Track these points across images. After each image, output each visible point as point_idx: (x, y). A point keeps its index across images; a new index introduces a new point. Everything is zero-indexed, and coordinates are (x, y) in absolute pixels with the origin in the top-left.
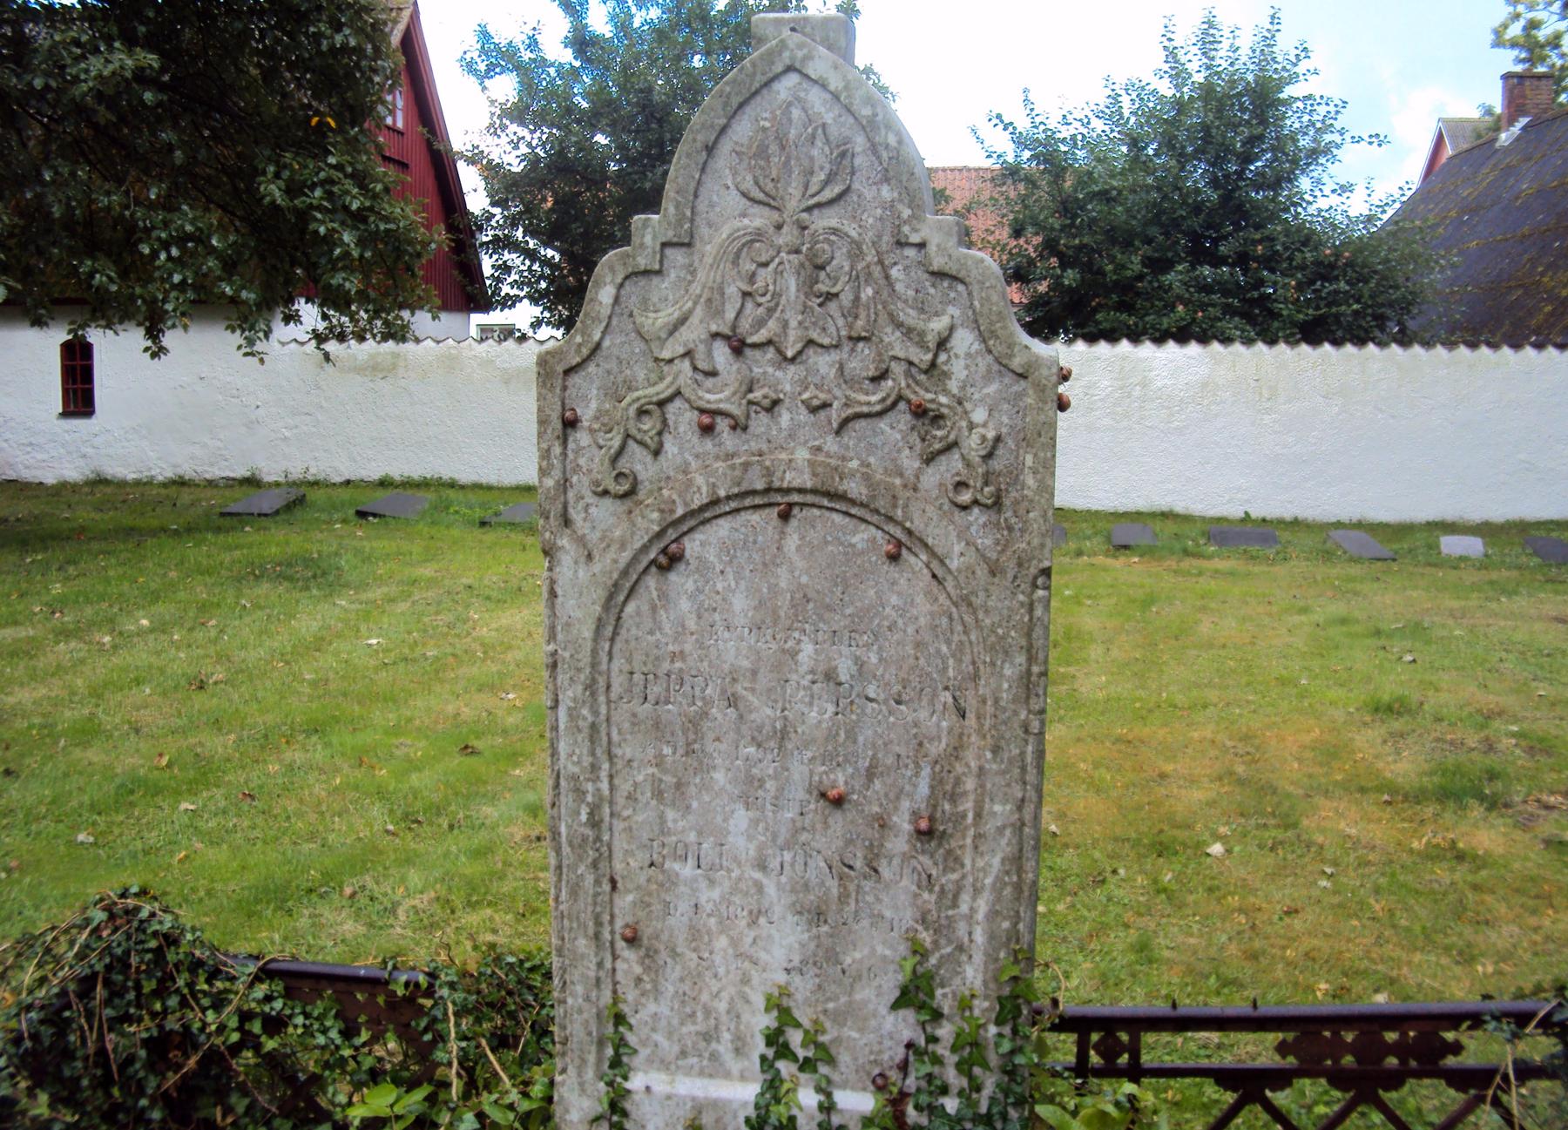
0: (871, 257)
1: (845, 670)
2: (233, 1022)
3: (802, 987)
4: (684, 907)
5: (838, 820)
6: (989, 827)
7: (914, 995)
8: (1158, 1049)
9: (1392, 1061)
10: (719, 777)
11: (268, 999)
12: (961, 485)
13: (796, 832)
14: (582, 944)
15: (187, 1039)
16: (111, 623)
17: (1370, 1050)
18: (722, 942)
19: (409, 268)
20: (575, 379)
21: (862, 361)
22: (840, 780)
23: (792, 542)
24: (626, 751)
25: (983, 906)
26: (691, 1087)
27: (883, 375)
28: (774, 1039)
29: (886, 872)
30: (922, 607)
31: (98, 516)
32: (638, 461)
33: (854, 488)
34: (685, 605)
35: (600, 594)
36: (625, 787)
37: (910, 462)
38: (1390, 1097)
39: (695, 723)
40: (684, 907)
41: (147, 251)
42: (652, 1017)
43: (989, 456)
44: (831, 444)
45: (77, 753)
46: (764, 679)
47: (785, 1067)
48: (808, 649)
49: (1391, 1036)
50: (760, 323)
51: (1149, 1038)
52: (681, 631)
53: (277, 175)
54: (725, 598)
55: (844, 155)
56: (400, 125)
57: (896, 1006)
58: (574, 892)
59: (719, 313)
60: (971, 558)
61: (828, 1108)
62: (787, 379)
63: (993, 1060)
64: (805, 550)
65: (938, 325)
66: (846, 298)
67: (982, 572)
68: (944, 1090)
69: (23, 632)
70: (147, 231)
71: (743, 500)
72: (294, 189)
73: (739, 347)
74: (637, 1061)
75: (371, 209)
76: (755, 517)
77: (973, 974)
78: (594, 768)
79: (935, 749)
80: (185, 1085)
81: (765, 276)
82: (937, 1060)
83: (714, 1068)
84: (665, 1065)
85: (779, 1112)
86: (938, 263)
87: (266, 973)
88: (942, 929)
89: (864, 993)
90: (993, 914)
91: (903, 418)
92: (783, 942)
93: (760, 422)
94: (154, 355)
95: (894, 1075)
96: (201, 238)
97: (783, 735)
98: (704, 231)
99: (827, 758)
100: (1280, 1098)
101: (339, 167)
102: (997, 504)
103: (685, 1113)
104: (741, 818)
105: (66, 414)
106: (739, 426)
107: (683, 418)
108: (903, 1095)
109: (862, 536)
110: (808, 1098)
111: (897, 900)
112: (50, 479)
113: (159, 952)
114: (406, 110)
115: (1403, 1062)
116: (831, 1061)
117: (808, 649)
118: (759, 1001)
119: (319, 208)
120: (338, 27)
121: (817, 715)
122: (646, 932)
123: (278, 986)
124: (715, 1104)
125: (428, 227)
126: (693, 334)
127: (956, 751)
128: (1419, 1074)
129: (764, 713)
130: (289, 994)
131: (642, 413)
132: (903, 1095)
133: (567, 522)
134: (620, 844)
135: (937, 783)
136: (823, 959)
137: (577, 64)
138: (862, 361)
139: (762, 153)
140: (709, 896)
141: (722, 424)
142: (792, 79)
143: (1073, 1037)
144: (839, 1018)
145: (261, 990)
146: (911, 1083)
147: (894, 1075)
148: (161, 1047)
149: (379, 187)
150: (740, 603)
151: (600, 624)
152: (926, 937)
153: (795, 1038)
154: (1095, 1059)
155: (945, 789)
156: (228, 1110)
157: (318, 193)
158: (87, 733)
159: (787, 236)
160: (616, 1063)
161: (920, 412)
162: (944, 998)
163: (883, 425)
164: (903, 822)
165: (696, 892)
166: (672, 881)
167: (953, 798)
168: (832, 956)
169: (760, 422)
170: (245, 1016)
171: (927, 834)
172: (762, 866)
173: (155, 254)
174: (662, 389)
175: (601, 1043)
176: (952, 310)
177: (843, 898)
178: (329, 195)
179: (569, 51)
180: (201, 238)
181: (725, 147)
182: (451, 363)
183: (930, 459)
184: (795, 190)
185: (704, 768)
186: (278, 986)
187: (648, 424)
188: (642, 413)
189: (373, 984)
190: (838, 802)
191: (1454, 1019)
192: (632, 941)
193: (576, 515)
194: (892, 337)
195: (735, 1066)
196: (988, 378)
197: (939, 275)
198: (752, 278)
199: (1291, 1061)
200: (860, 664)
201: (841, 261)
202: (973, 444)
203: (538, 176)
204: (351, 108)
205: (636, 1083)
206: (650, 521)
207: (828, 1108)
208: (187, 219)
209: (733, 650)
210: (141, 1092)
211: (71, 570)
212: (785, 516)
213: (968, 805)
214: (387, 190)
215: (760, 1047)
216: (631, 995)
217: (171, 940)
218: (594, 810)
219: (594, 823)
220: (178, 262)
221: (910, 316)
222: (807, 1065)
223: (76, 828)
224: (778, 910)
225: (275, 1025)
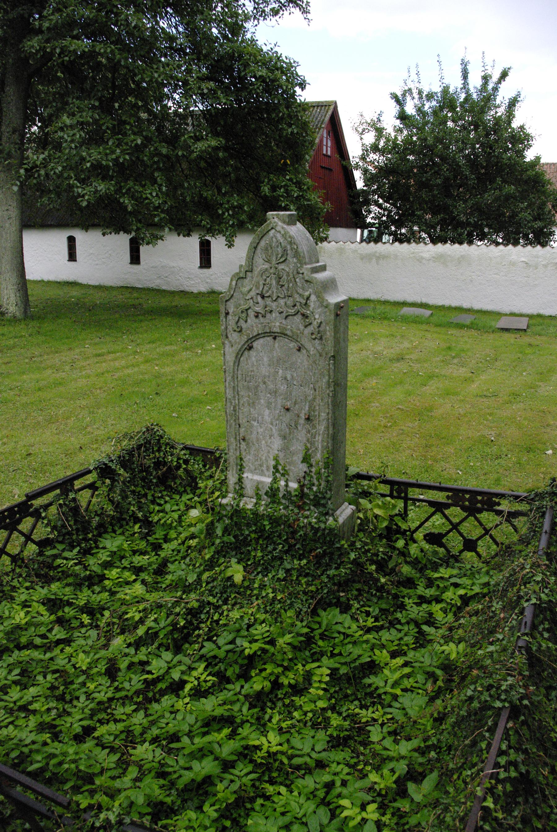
0: (291, 276)
1: (289, 377)
2: (175, 459)
3: (281, 455)
4: (255, 432)
5: (288, 414)
6: (321, 418)
7: (306, 459)
8: (413, 493)
9: (479, 505)
10: (262, 401)
11: (185, 454)
12: (312, 334)
13: (279, 416)
14: (232, 440)
15: (165, 464)
16: (202, 346)
17: (473, 500)
18: (263, 442)
19: (317, 218)
20: (228, 303)
21: (290, 302)
22: (288, 404)
23: (277, 345)
24: (241, 393)
25: (320, 438)
26: (257, 478)
27: (294, 306)
28: (275, 467)
29: (299, 428)
30: (306, 363)
31: (209, 306)
32: (242, 323)
33: (289, 333)
34: (254, 359)
35: (234, 355)
36: (242, 402)
37: (302, 327)
38: (478, 516)
39: (257, 387)
40: (255, 432)
41: (220, 212)
42: (248, 459)
43: (319, 327)
44: (284, 321)
45: (180, 389)
46: (271, 379)
47: (278, 475)
48: (281, 371)
49: (479, 498)
50: (267, 292)
51: (410, 489)
52: (253, 365)
53: (268, 183)
54: (262, 357)
55: (285, 250)
56: (329, 153)
57: (302, 462)
58: (231, 426)
59: (258, 288)
60: (315, 351)
61: (287, 486)
62: (274, 305)
63: (324, 478)
64: (280, 347)
65: (307, 294)
66: (286, 286)
67: (318, 355)
68: (313, 485)
69: (174, 347)
70: (221, 205)
71: (265, 334)
72: (274, 188)
73: (263, 297)
74: (245, 470)
75: (302, 196)
76: (268, 338)
77: (319, 456)
78: (234, 397)
79: (310, 398)
80: (164, 474)
81: (268, 279)
82: (312, 477)
83: (262, 474)
84: (251, 472)
85: (276, 486)
86: (306, 278)
87: (185, 448)
88: (312, 443)
89: (295, 458)
90: (323, 441)
91: (299, 317)
92: (277, 443)
93: (268, 315)
94: (229, 247)
95: (302, 480)
96: (240, 207)
97: (276, 392)
98: (255, 268)
99: (285, 399)
100: (447, 512)
101: (291, 180)
102: (321, 338)
103: (255, 484)
104: (267, 412)
105: (201, 267)
106: (264, 316)
107: (251, 313)
108: (304, 485)
109: (292, 345)
110: (283, 483)
111: (302, 435)
112: (195, 291)
113: (159, 440)
114: (331, 147)
115: (483, 506)
116: (288, 475)
117: (281, 371)
118: (272, 457)
119: (282, 196)
120: (290, 125)
121: (283, 388)
122: (247, 438)
123: (188, 452)
124: (262, 482)
125: (323, 204)
126: (253, 293)
127: (314, 399)
128: (487, 510)
129: (271, 386)
130: (191, 454)
131: (242, 312)
132: (304, 485)
133: (227, 337)
134: (241, 416)
135: (310, 407)
136: (285, 449)
137: (401, 126)
138: (290, 302)
139: (266, 249)
140: (261, 430)
141: (260, 316)
142: (273, 231)
143: (389, 486)
144: (290, 464)
145: (183, 452)
146: (306, 482)
147: (302, 480)
148: (158, 464)
149: (305, 187)
150: (265, 359)
151: (235, 363)
152: (309, 445)
153: (280, 468)
154: (395, 494)
155: (312, 408)
156: (175, 483)
157: (282, 190)
158: (184, 383)
159: (272, 271)
160: (240, 470)
161: (303, 315)
162: (313, 461)
163: (295, 317)
164: (303, 416)
165: (258, 430)
166: (252, 426)
167: (314, 411)
168: (288, 448)
169: (268, 315)
170: (179, 459)
171: (308, 419)
172: (272, 424)
173: (223, 213)
174: (246, 307)
175: (237, 465)
176: (311, 290)
177: (290, 433)
178: (287, 191)
179: (398, 121)
180: (240, 207)
181: (259, 247)
182: (341, 251)
183: (306, 326)
184: (274, 259)
185: (259, 399)
186: (188, 452)
187: (244, 315)
188: (242, 312)
189: (212, 453)
190: (288, 410)
191: (497, 495)
192: (244, 439)
193: (229, 336)
194: (296, 296)
195: (267, 473)
196: (319, 307)
197: (307, 281)
198: (265, 280)
199: (450, 501)
200: (292, 376)
201: (285, 277)
202: (315, 323)
203: (385, 171)
204: (296, 156)
205: (245, 475)
206: (245, 338)
207: (287, 486)
208: (235, 200)
209: (264, 370)
210: (151, 475)
211: (194, 326)
212: (275, 338)
213: (317, 413)
214: (308, 188)
215: (272, 470)
216: (244, 454)
217: (161, 437)
218: (234, 407)
219: (235, 410)
220: (232, 216)
221: (300, 291)
222: (283, 475)
223: (173, 412)
224: (276, 435)
225: (186, 462)
